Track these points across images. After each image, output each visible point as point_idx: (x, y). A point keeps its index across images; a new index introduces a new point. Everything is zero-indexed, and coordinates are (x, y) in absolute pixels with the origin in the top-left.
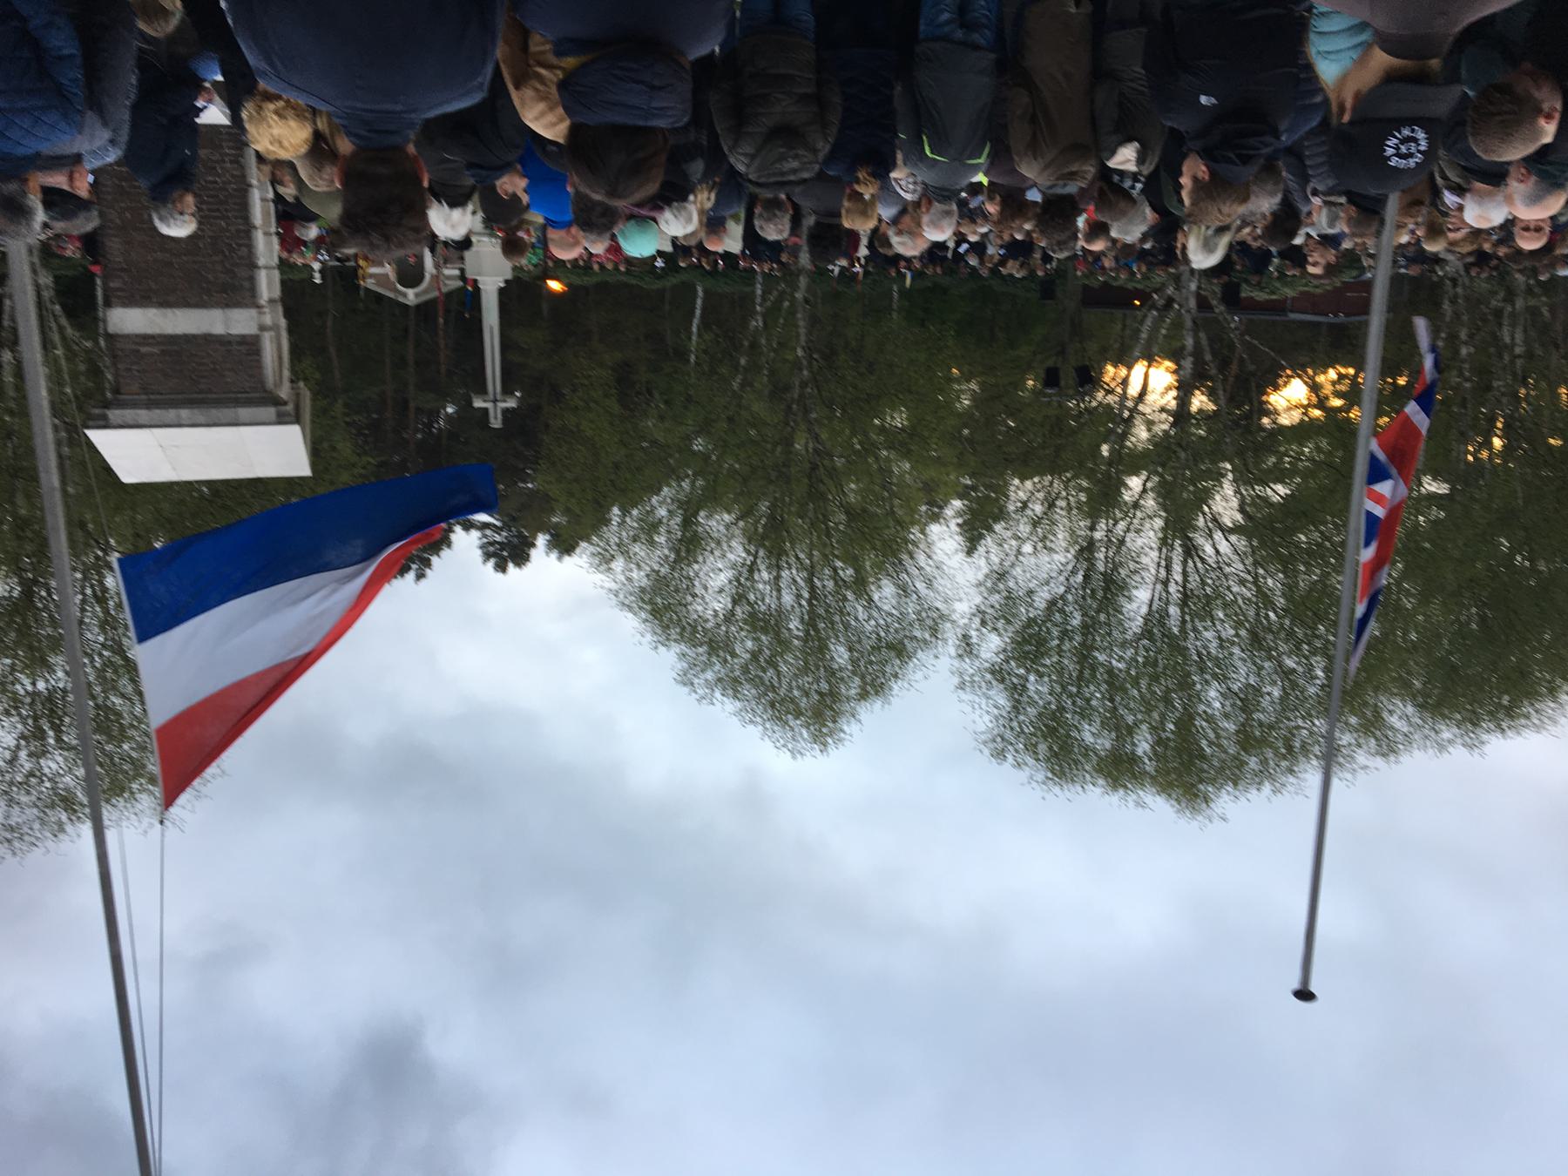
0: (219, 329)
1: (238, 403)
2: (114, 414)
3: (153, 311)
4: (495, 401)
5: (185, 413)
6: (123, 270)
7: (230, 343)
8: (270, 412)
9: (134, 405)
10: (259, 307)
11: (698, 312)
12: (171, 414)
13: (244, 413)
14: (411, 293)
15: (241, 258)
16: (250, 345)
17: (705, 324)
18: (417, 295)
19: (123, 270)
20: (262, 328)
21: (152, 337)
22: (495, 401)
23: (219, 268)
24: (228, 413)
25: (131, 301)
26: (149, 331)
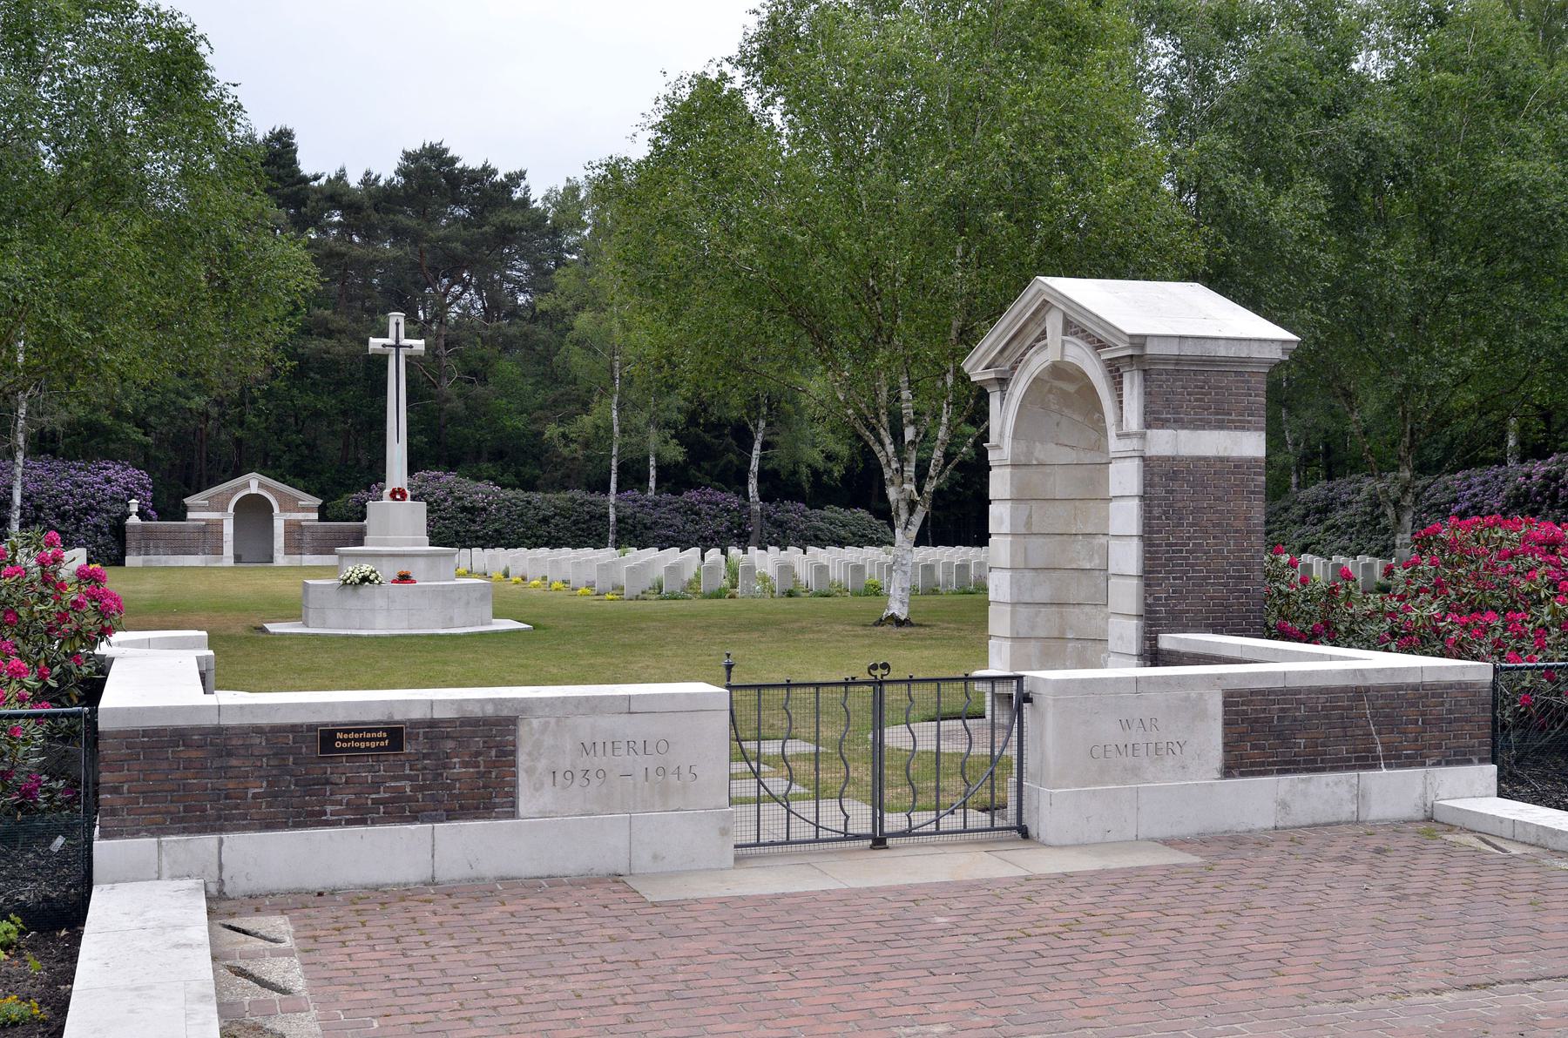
0: (1184, 434)
1: (1178, 360)
2: (1276, 354)
3: (1234, 454)
4: (398, 346)
5: (1222, 351)
6: (1253, 492)
7: (1175, 421)
8: (1152, 349)
9: (1260, 361)
10: (1143, 458)
11: (653, 472)
12: (1232, 352)
13: (1172, 350)
15: (1159, 506)
16: (1153, 418)
18: (248, 485)
19: (1253, 492)
20: (1143, 436)
22: (398, 346)
23: (1179, 496)
24: (1189, 350)
25: (1239, 466)
26: (1239, 433)
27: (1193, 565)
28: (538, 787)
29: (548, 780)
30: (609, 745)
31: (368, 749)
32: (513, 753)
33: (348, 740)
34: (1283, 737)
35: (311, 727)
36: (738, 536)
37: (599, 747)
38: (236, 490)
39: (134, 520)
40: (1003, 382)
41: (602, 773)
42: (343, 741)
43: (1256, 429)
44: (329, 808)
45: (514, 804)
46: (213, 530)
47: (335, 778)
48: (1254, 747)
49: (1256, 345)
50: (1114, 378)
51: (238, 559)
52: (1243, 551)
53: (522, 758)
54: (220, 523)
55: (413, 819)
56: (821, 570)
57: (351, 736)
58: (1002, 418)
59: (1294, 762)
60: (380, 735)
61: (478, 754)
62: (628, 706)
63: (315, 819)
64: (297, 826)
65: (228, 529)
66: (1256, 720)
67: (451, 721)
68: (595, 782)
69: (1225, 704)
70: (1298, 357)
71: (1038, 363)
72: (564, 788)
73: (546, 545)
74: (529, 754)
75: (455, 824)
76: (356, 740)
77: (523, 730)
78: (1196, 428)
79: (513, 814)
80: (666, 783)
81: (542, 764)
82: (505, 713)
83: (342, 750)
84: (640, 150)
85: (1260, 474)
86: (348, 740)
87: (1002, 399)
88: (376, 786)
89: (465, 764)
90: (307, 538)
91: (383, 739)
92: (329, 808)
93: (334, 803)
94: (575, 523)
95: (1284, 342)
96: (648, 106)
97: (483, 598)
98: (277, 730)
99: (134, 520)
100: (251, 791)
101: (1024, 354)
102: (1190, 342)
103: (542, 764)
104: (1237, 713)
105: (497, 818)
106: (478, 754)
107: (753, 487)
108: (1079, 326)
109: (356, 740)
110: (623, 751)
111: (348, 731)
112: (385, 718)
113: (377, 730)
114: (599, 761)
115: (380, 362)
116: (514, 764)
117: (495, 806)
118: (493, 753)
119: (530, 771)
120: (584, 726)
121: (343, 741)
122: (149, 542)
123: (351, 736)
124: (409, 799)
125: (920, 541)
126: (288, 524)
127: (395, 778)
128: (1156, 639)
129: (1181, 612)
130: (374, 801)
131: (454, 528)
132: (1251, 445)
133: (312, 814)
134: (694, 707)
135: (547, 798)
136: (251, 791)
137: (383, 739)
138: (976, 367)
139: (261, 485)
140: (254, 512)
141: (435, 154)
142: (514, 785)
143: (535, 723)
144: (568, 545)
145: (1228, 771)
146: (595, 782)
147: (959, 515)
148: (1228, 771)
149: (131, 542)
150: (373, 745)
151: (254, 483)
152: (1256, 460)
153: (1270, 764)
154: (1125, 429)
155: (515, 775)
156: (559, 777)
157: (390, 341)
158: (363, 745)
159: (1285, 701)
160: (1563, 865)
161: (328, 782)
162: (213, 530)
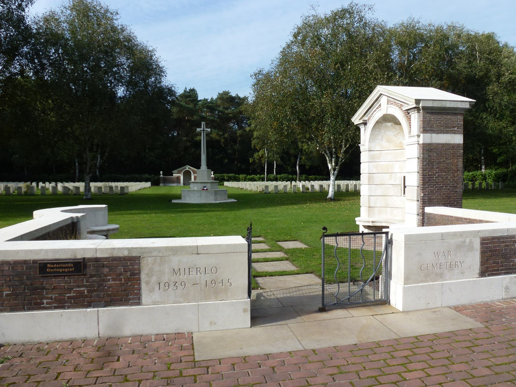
0: (434, 135)
4: (204, 130)
6: (459, 156)
7: (431, 131)
14: (187, 169)
17: (199, 143)
18: (186, 168)
19: (459, 156)
21: (453, 133)
22: (204, 130)
26: (453, 135)
27: (437, 182)
28: (152, 291)
29: (157, 287)
30: (187, 271)
31: (64, 272)
32: (139, 274)
33: (53, 268)
34: (506, 257)
35: (35, 262)
37: (182, 271)
38: (183, 169)
40: (365, 124)
41: (183, 284)
42: (51, 268)
43: (460, 134)
44: (45, 301)
45: (139, 299)
47: (47, 286)
48: (494, 263)
49: (461, 103)
50: (407, 117)
51: (184, 184)
52: (455, 177)
53: (143, 277)
55: (89, 306)
57: (55, 266)
58: (365, 135)
59: (512, 269)
60: (70, 265)
61: (121, 274)
62: (196, 251)
63: (38, 306)
64: (29, 309)
65: (182, 178)
66: (495, 251)
67: (106, 259)
68: (180, 288)
69: (482, 244)
70: (473, 106)
71: (377, 115)
72: (165, 290)
74: (147, 274)
75: (109, 308)
76: (57, 268)
77: (143, 263)
78: (438, 133)
79: (139, 303)
80: (214, 288)
81: (154, 279)
82: (134, 255)
83: (50, 273)
85: (461, 149)
86: (53, 268)
87: (365, 130)
88: (70, 290)
89: (114, 280)
91: (71, 267)
92: (45, 301)
93: (47, 298)
95: (470, 102)
98: (16, 263)
99: (161, 176)
100: (5, 293)
101: (372, 114)
102: (282, 240)
103: (154, 279)
104: (487, 248)
105: (131, 305)
106: (121, 274)
108: (392, 101)
109: (57, 268)
110: (194, 272)
111: (53, 264)
112: (73, 257)
113: (68, 263)
114: (183, 277)
116: (139, 279)
117: (130, 299)
118: (129, 273)
119: (148, 283)
120: (175, 261)
121: (51, 268)
123: (55, 266)
124: (86, 296)
125: (337, 179)
127: (78, 287)
128: (424, 209)
129: (433, 199)
130: (69, 297)
132: (458, 139)
133: (36, 304)
134: (232, 250)
135: (156, 296)
136: (5, 293)
137: (71, 267)
138: (356, 120)
139: (189, 168)
141: (226, 93)
142: (140, 289)
143: (150, 260)
145: (483, 273)
146: (180, 288)
147: (351, 169)
148: (483, 273)
150: (66, 270)
151: (187, 168)
152: (459, 145)
153: (501, 270)
154: (412, 135)
155: (139, 284)
156: (162, 285)
157: (202, 129)
158: (61, 270)
159: (507, 242)
161: (44, 288)
162: (178, 178)
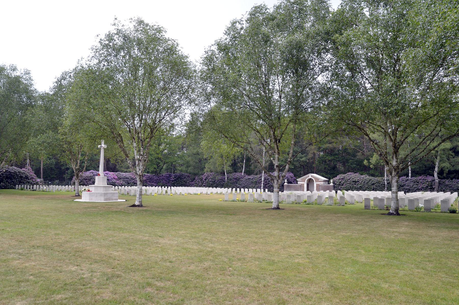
18: (309, 176)
36: (430, 188)
38: (307, 177)
39: (286, 184)
46: (302, 186)
54: (303, 184)
56: (352, 197)
73: (373, 190)
84: (43, 84)
90: (321, 188)
94: (382, 185)
96: (185, 54)
97: (101, 195)
107: (436, 174)
115: (100, 149)
122: (289, 188)
126: (317, 185)
131: (111, 183)
139: (312, 176)
140: (310, 181)
144: (378, 190)
149: (285, 188)
151: (310, 176)
160: (457, 292)
162: (302, 186)
